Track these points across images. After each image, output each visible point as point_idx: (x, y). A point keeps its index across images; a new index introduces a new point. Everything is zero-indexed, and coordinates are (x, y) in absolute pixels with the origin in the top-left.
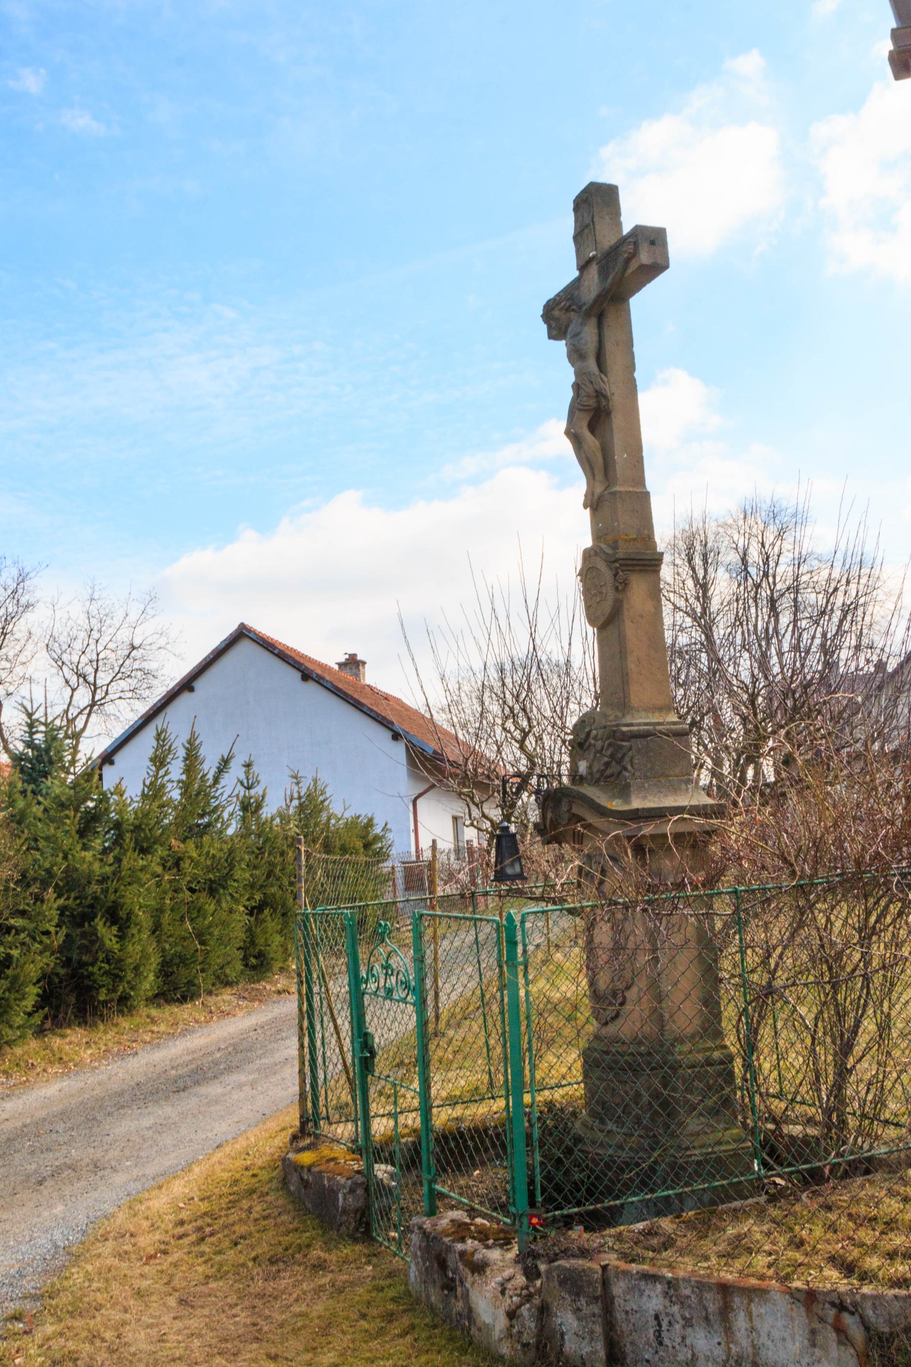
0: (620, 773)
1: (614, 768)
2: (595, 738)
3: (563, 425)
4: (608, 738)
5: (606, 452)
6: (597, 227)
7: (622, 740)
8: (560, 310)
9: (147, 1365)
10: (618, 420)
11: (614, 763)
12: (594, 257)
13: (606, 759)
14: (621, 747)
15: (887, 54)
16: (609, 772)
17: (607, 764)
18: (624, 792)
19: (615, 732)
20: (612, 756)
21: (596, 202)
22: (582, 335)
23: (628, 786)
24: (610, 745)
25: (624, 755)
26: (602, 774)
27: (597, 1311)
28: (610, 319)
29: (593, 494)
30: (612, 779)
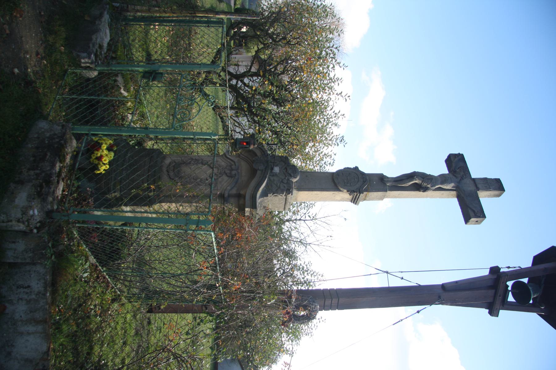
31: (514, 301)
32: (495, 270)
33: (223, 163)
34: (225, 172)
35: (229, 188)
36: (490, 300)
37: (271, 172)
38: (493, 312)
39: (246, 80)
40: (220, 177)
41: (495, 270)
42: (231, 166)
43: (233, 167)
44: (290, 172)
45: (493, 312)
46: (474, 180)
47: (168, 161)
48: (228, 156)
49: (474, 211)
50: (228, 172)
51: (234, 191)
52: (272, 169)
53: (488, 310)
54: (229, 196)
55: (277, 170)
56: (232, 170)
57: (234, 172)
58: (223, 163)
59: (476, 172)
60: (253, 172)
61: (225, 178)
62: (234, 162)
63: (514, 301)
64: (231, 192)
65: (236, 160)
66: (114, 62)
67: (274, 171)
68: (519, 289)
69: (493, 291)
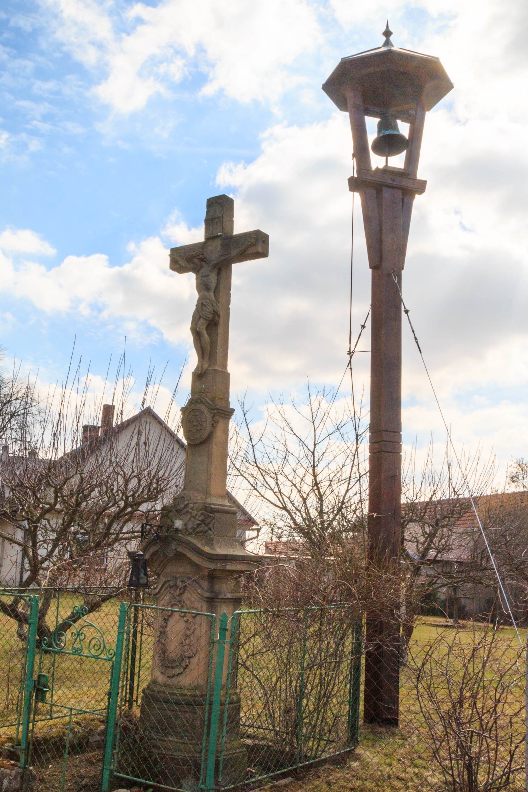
0: (206, 531)
1: (203, 528)
2: (192, 509)
3: (189, 325)
4: (201, 510)
5: (213, 344)
6: (224, 220)
7: (210, 513)
8: (199, 259)
9: (1, 748)
10: (220, 330)
11: (203, 525)
12: (220, 236)
13: (199, 522)
14: (209, 516)
15: (423, 195)
16: (199, 529)
17: (198, 525)
18: (210, 542)
19: (206, 507)
20: (203, 521)
21: (219, 208)
22: (210, 277)
23: (212, 540)
24: (202, 514)
25: (211, 521)
26: (194, 531)
27: (241, 727)
28: (223, 273)
29: (202, 367)
30: (201, 534)
31: (406, 151)
32: (355, 184)
33: (167, 598)
34: (179, 596)
35: (199, 591)
36: (399, 193)
37: (181, 531)
38: (421, 187)
39: (42, 552)
40: (184, 602)
41: (355, 184)
42: (171, 587)
43: (171, 584)
44: (182, 506)
45: (421, 187)
46: (208, 239)
47: (161, 679)
48: (158, 589)
49: (250, 246)
50: (178, 592)
51: (205, 584)
52: (177, 530)
53: (417, 196)
54: (211, 591)
55: (178, 524)
56: (176, 586)
57: (179, 583)
58: (167, 598)
59: (197, 235)
60: (180, 557)
61: (186, 595)
62: (165, 582)
63: (406, 151)
64: (206, 589)
65: (163, 580)
66: (401, 249)
67: (180, 528)
68: (389, 143)
69: (384, 189)
